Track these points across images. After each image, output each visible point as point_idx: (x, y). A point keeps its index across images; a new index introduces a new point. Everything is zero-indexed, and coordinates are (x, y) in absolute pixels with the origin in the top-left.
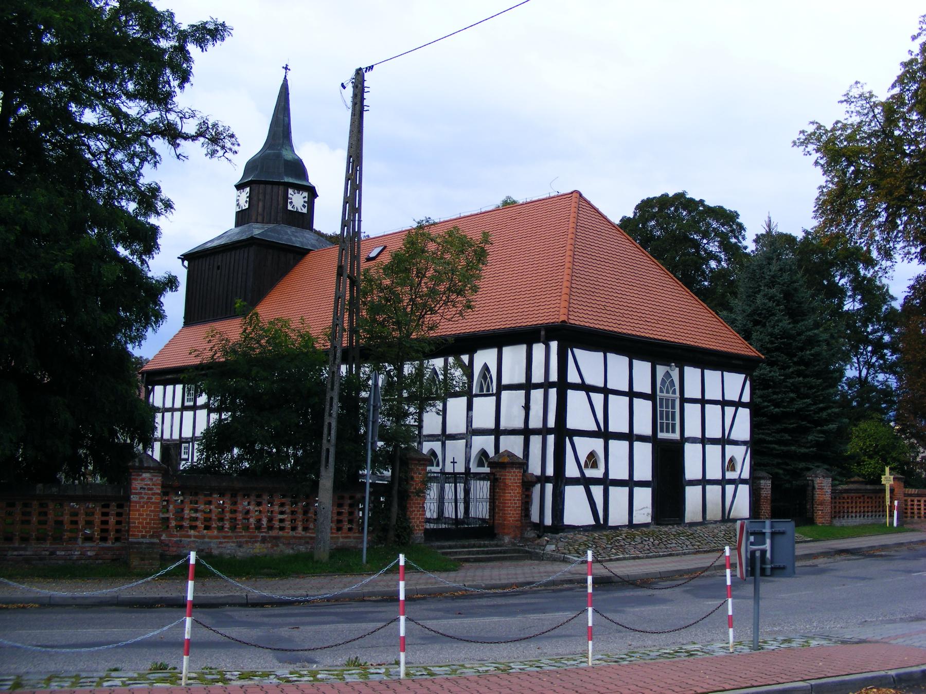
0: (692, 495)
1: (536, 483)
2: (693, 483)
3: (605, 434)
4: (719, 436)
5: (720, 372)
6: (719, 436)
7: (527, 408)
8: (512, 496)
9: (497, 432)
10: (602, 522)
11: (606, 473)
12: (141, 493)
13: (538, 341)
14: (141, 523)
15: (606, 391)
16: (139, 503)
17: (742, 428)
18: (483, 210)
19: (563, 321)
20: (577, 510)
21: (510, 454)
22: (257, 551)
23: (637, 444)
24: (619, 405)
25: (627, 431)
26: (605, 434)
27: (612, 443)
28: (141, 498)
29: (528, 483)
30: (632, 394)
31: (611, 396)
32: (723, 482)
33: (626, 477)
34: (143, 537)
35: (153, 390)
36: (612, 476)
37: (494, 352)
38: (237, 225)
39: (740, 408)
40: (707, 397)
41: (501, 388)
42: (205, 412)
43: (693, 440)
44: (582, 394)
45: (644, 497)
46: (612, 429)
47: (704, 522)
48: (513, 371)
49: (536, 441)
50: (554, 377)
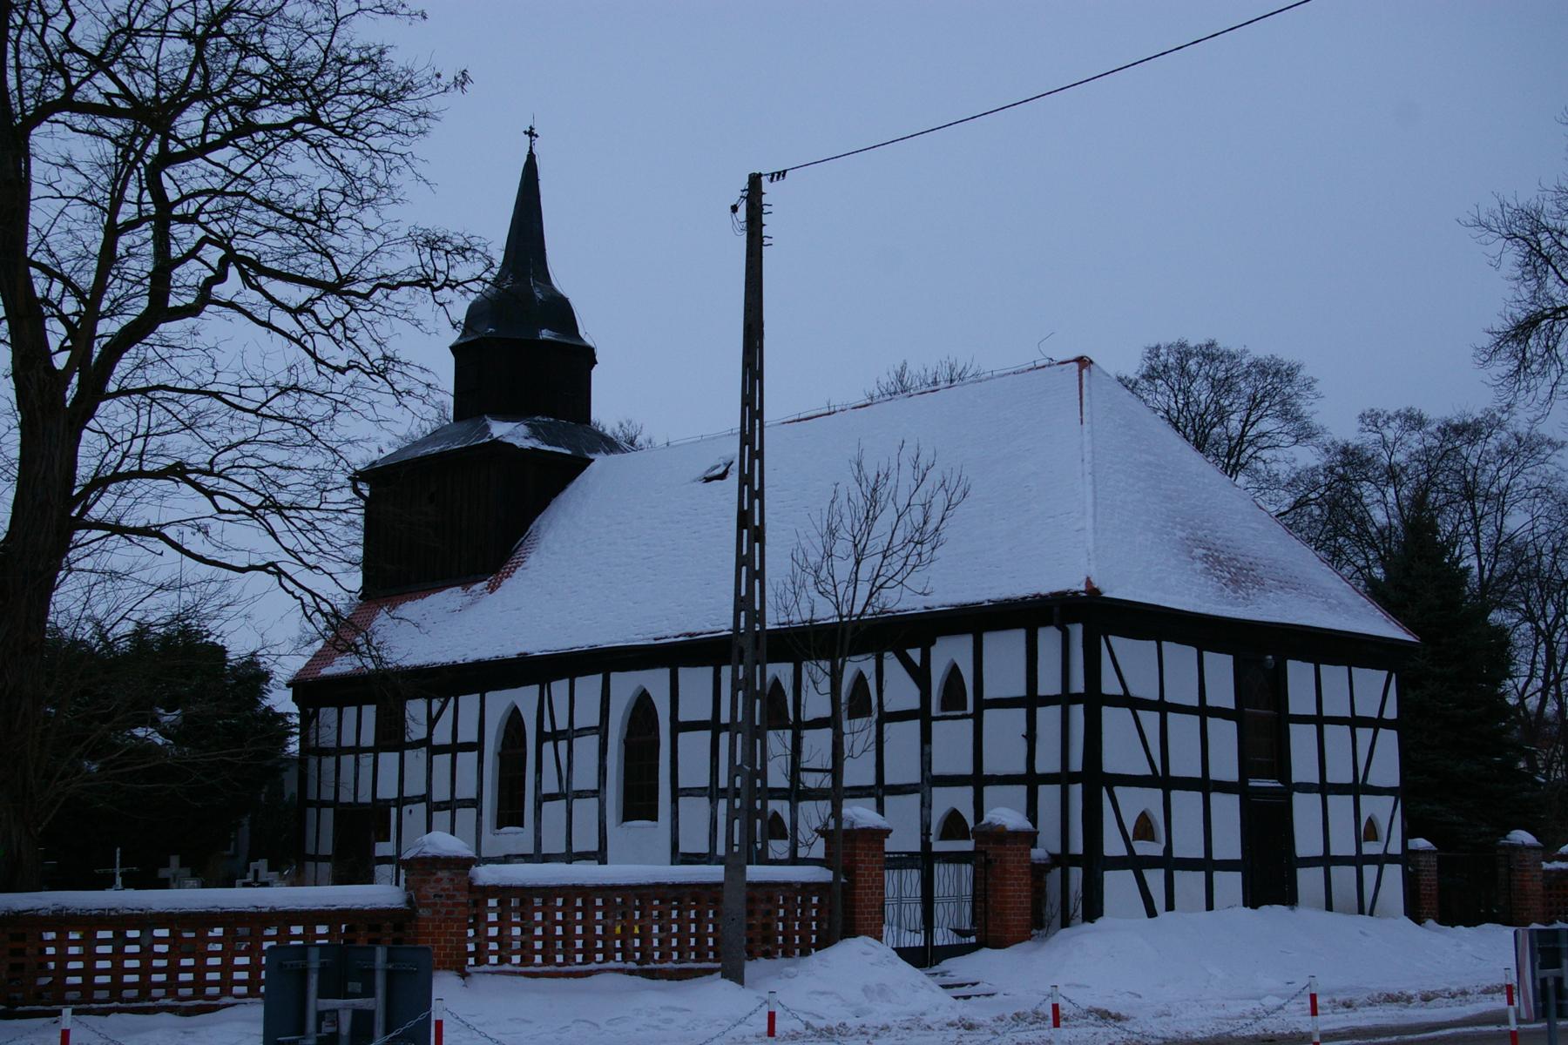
1: (1053, 866)
2: (1310, 862)
3: (1163, 781)
4: (1349, 779)
5: (1345, 668)
6: (1349, 779)
7: (1031, 737)
9: (978, 780)
11: (1168, 848)
12: (435, 904)
15: (1163, 707)
17: (1386, 769)
24: (1184, 729)
26: (1163, 781)
27: (1175, 795)
30: (1204, 711)
31: (1170, 715)
32: (1359, 861)
33: (1200, 854)
35: (316, 714)
37: (967, 641)
39: (1381, 730)
40: (1326, 713)
41: (982, 704)
42: (422, 753)
43: (1306, 788)
44: (1126, 713)
46: (1173, 772)
49: (1049, 795)
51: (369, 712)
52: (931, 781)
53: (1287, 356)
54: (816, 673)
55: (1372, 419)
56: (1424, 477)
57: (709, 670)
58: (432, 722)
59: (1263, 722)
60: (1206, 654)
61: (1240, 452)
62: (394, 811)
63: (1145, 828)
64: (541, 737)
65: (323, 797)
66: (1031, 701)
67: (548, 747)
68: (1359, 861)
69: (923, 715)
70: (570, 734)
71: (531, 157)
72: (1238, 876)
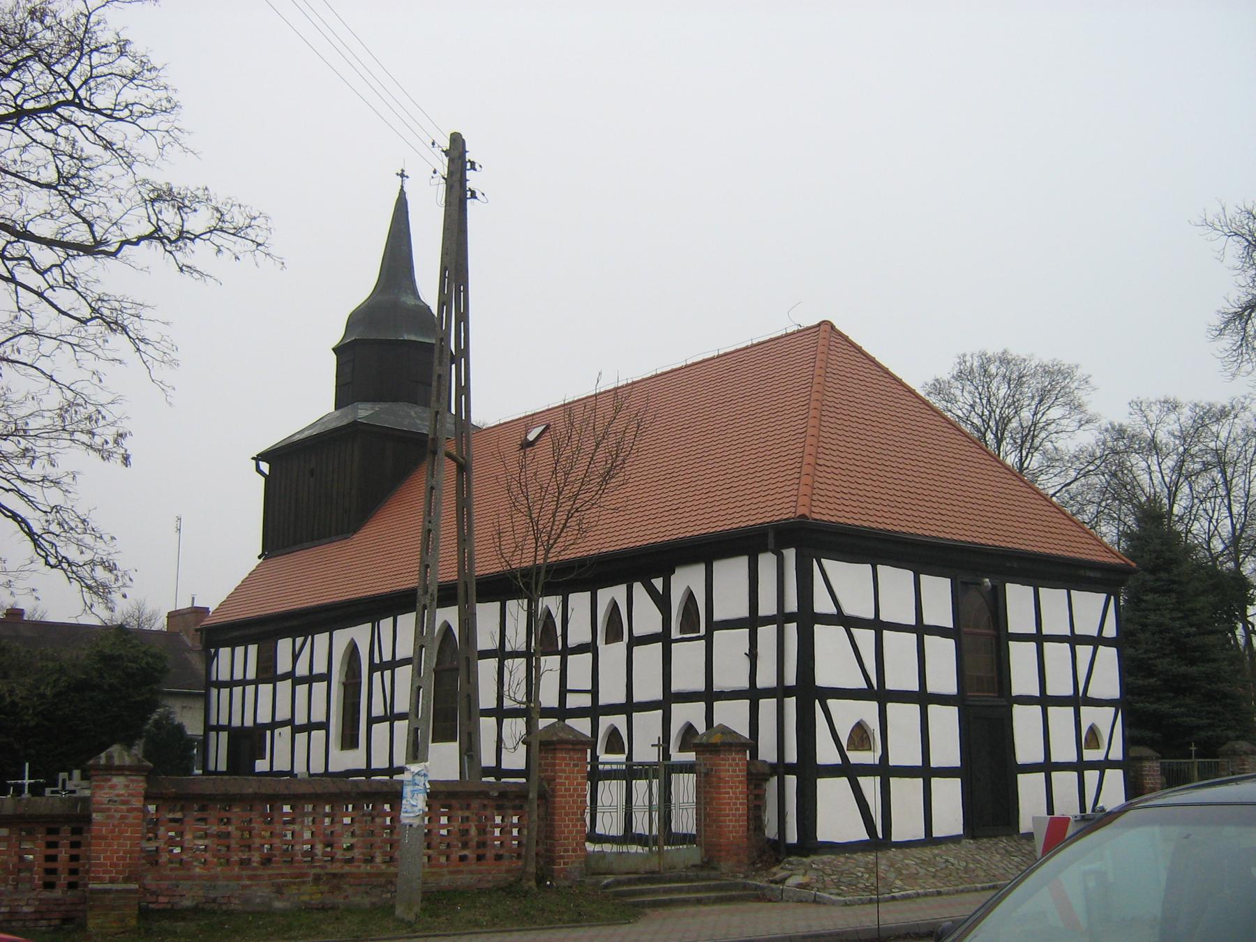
0: (1030, 788)
1: (771, 775)
3: (880, 695)
4: (1069, 691)
6: (1069, 691)
7: (753, 655)
8: (734, 797)
9: (709, 696)
10: (880, 836)
12: (109, 809)
13: (765, 550)
14: (111, 858)
15: (878, 625)
16: (107, 825)
17: (1106, 677)
18: (689, 362)
19: (803, 516)
20: (837, 816)
21: (725, 730)
22: (306, 898)
23: (933, 709)
24: (900, 647)
25: (1050, 709)
26: (880, 695)
28: (108, 817)
29: (757, 776)
30: (921, 629)
32: (1080, 766)
34: (112, 881)
35: (216, 654)
36: (893, 761)
38: (338, 406)
45: (948, 794)
46: (890, 685)
47: (930, 840)
48: (730, 603)
49: (767, 707)
50: (792, 605)
51: (253, 649)
52: (670, 698)
53: (1066, 360)
54: (578, 602)
55: (1139, 407)
56: (1181, 449)
57: (498, 604)
58: (295, 657)
59: (983, 641)
60: (922, 577)
61: (1034, 437)
62: (268, 733)
63: (860, 736)
64: (373, 668)
65: (221, 723)
66: (753, 622)
67: (377, 675)
68: (1080, 766)
69: (664, 638)
70: (394, 664)
71: (402, 194)
72: (957, 782)
